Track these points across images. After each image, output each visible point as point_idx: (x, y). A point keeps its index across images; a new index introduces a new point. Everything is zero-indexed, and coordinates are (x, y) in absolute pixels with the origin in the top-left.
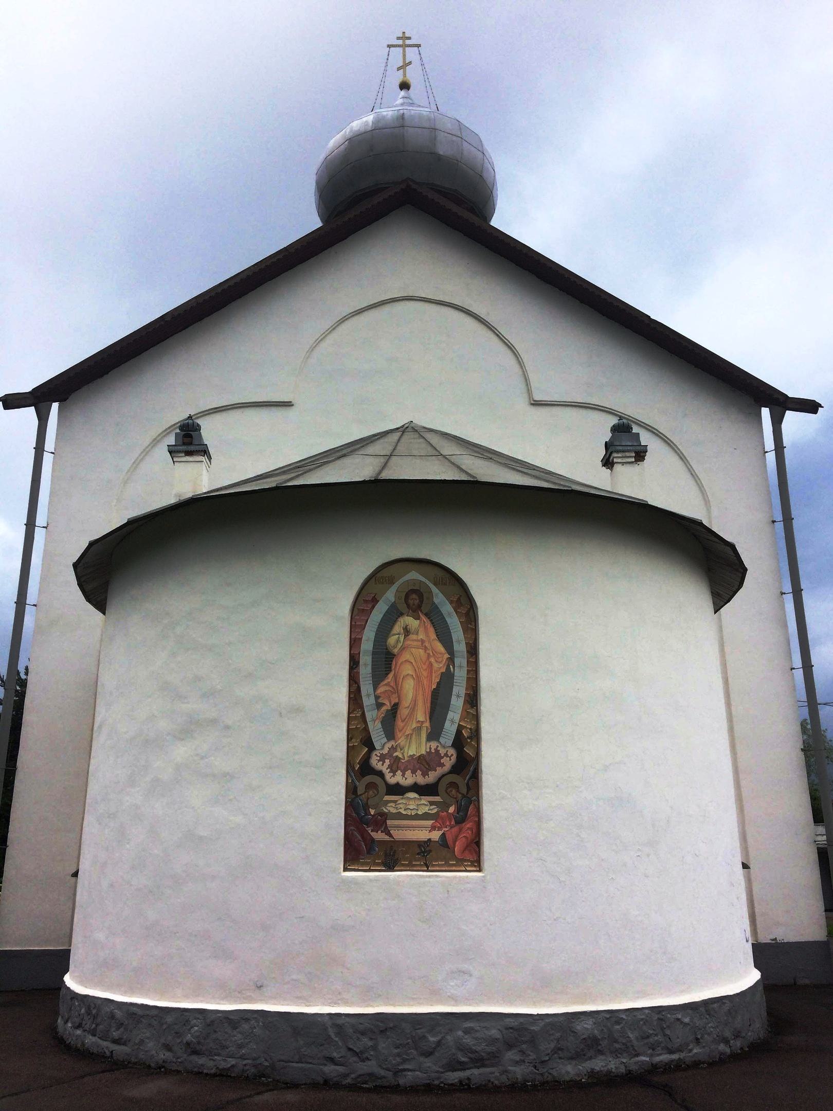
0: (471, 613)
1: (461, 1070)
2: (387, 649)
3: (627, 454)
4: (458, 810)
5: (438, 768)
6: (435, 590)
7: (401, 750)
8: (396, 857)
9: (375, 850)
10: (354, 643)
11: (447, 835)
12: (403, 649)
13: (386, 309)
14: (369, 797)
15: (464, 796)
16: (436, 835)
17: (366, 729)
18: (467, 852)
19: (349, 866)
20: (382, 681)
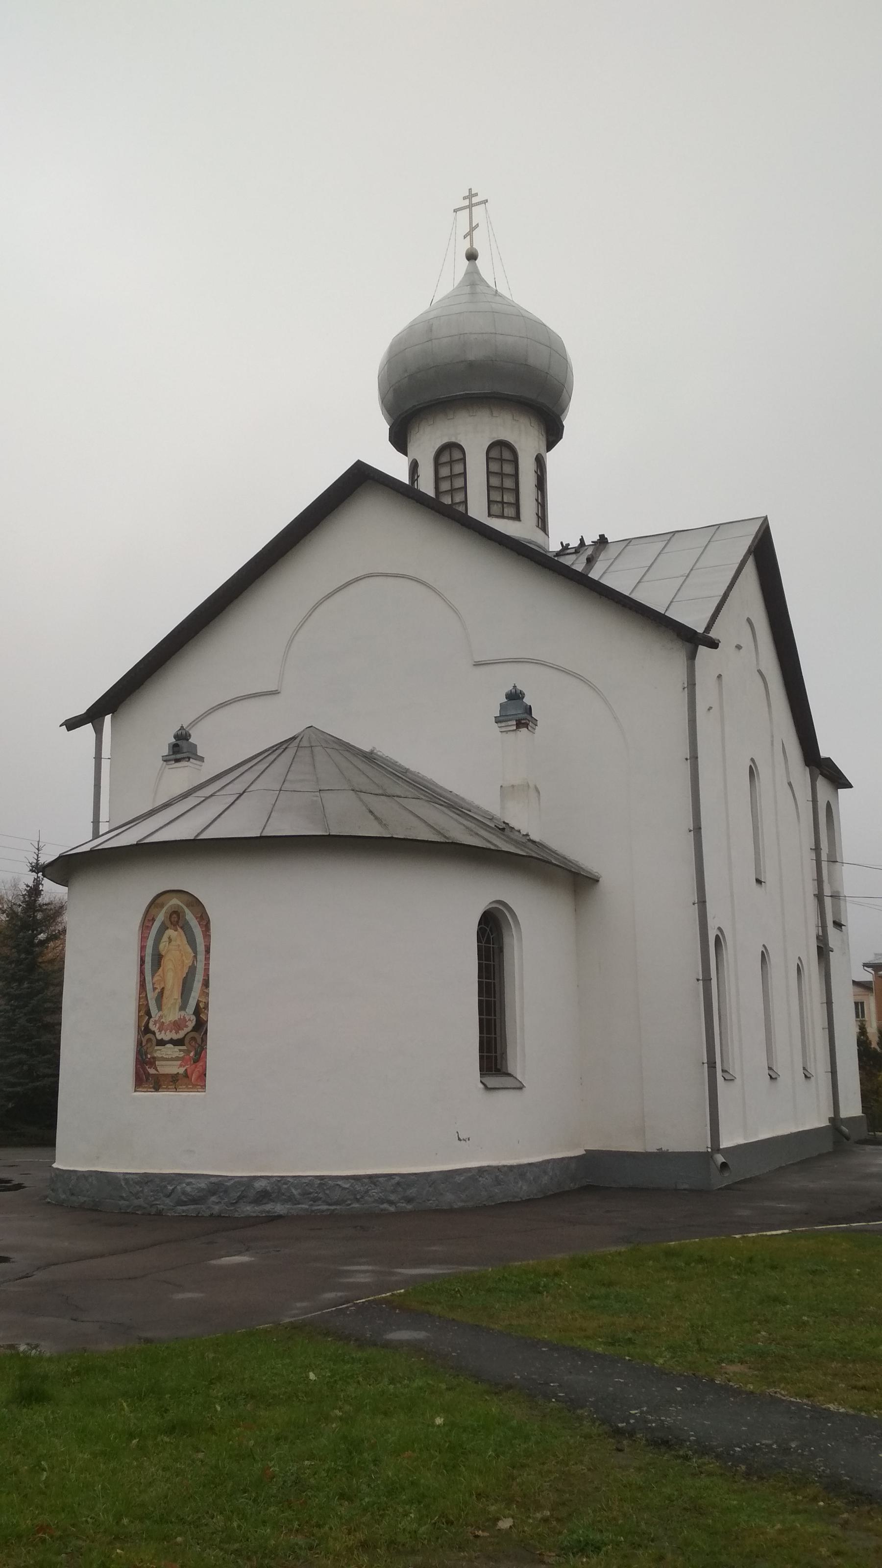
1: (185, 1206)
3: (510, 723)
4: (195, 1055)
5: (184, 1028)
6: (187, 911)
8: (160, 1084)
9: (149, 1079)
10: (143, 948)
12: (168, 951)
13: (351, 589)
16: (181, 1071)
17: (147, 1005)
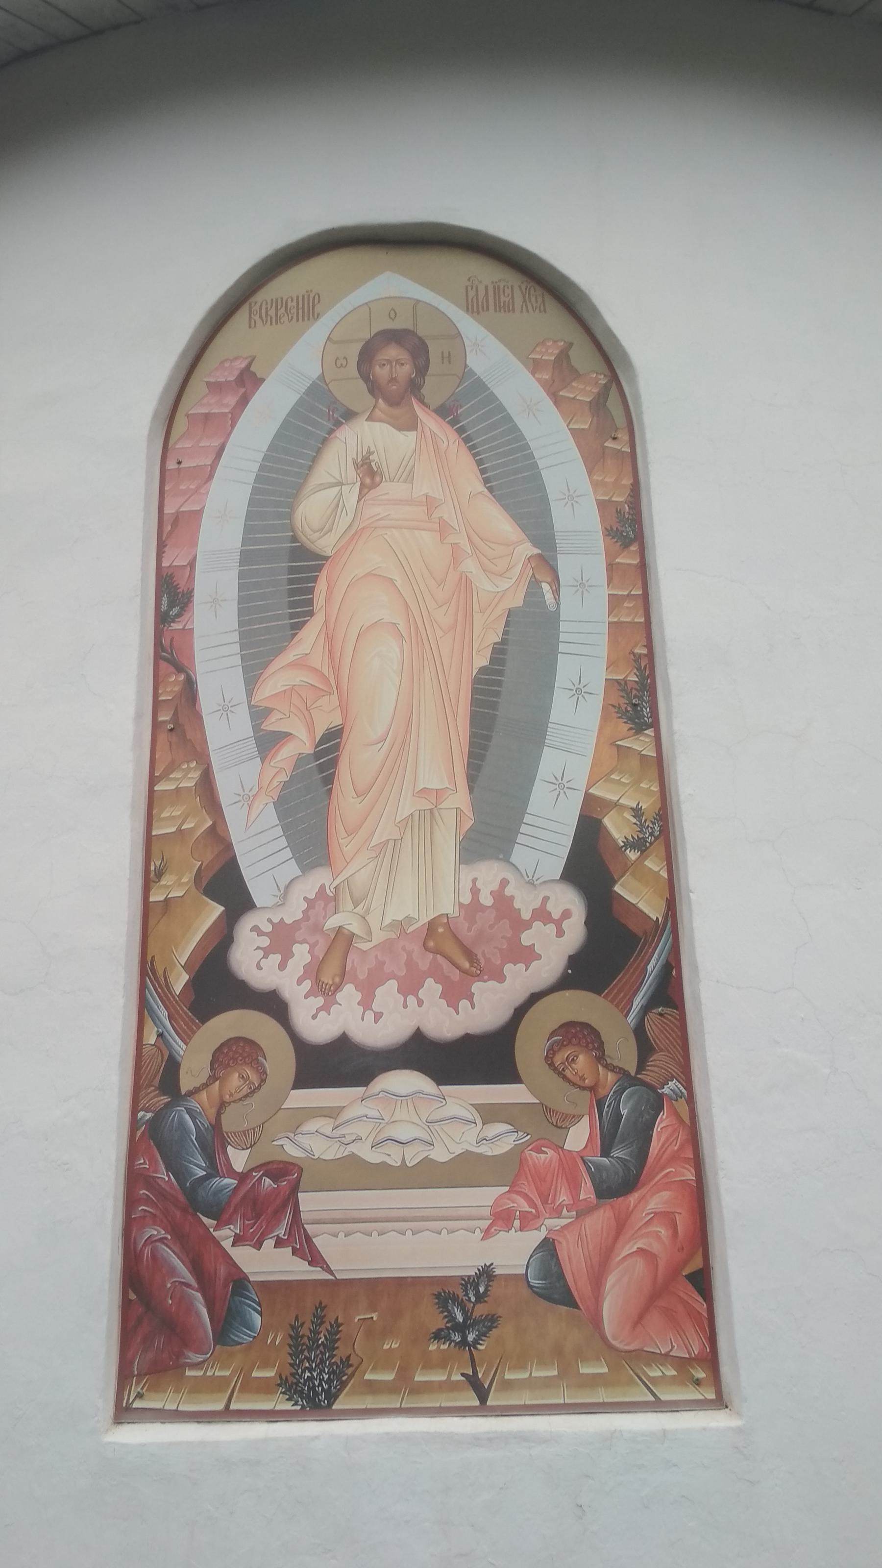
0: (613, 404)
2: (294, 539)
5: (508, 968)
7: (356, 904)
8: (341, 1352)
11: (563, 1254)
14: (227, 1098)
15: (627, 1080)
18: (655, 1319)
19: (140, 1396)
20: (279, 651)
